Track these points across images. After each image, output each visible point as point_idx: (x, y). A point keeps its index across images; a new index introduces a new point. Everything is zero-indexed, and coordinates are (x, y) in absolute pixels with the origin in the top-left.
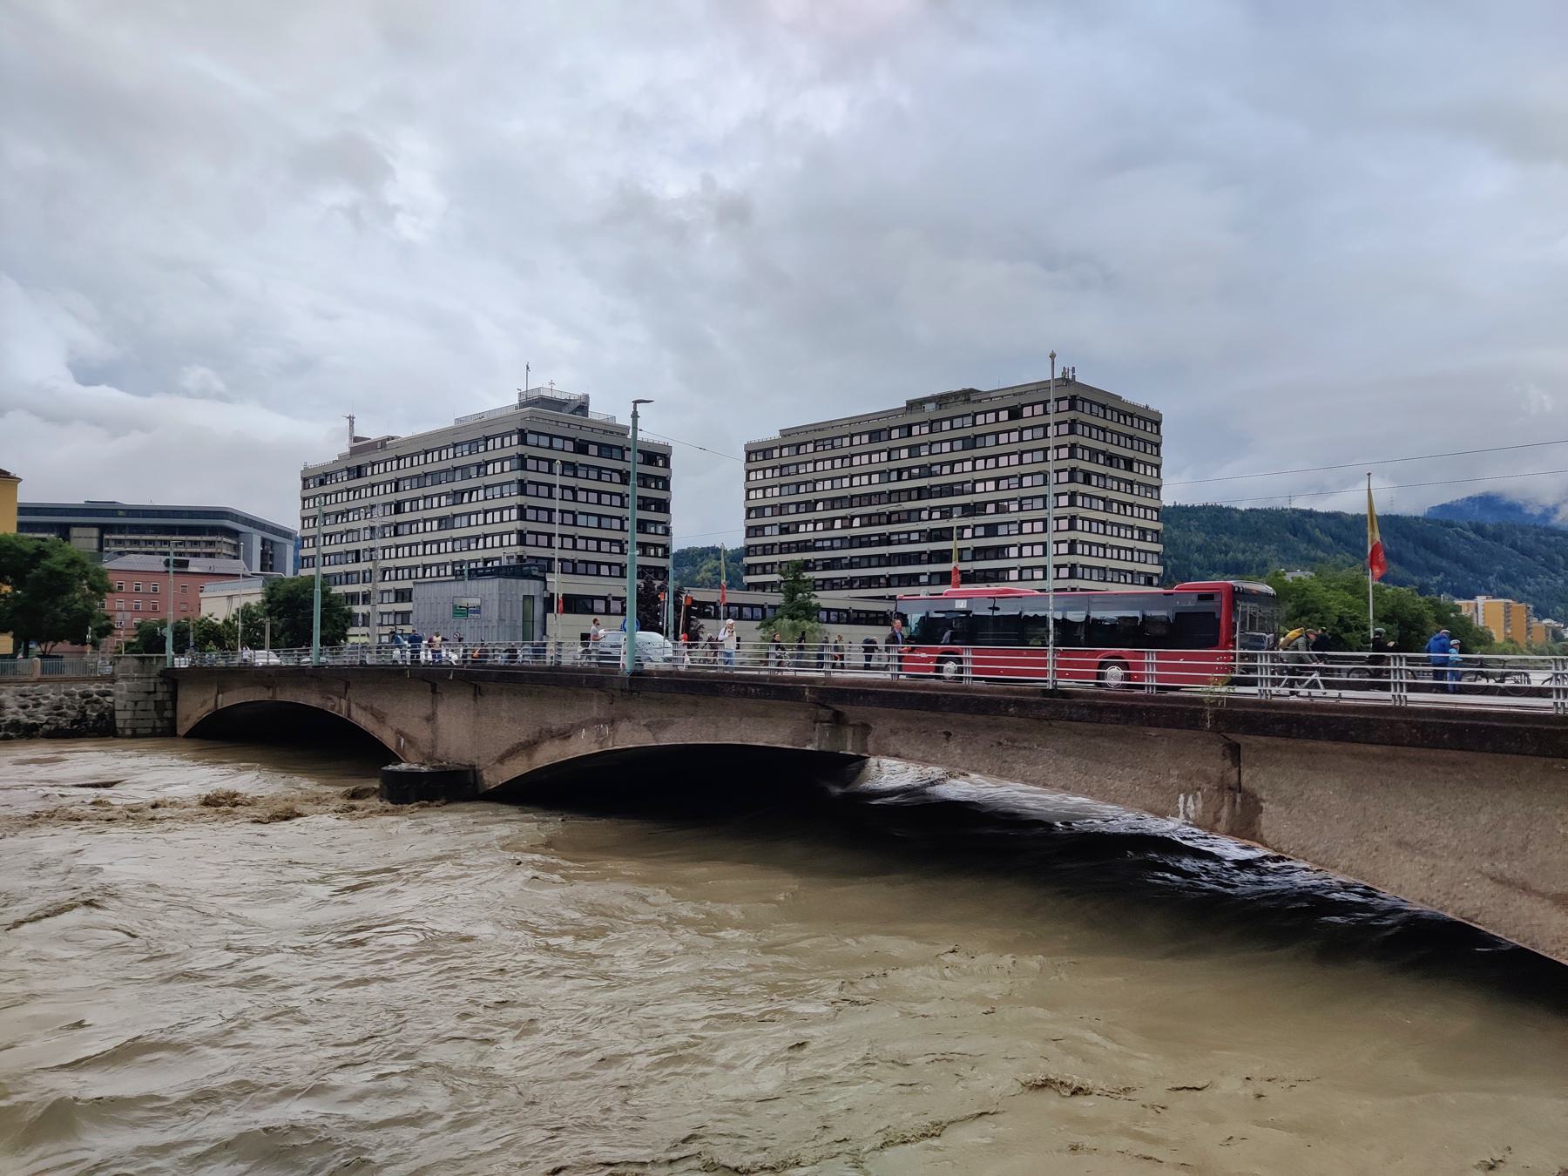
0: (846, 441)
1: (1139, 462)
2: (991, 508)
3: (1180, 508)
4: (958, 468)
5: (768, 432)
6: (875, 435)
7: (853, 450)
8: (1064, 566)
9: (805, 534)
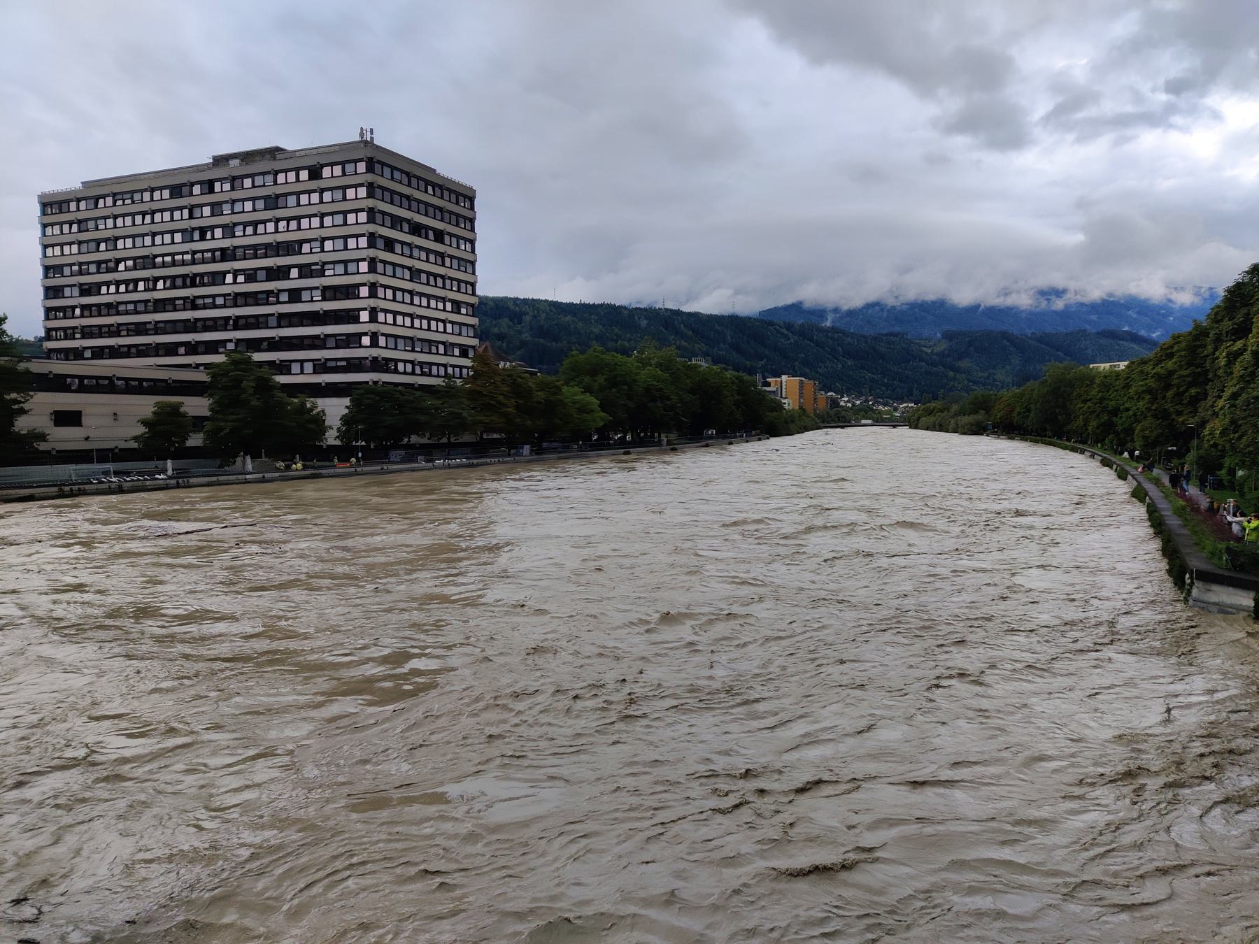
0: (147, 196)
1: (451, 235)
2: (294, 273)
3: (584, 305)
4: (261, 228)
5: (69, 180)
6: (176, 191)
7: (155, 206)
9: (106, 296)
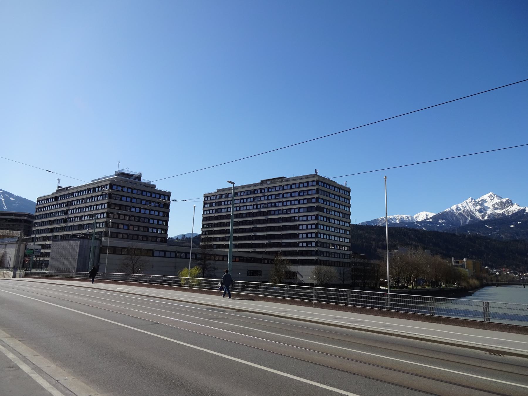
8: (301, 247)
